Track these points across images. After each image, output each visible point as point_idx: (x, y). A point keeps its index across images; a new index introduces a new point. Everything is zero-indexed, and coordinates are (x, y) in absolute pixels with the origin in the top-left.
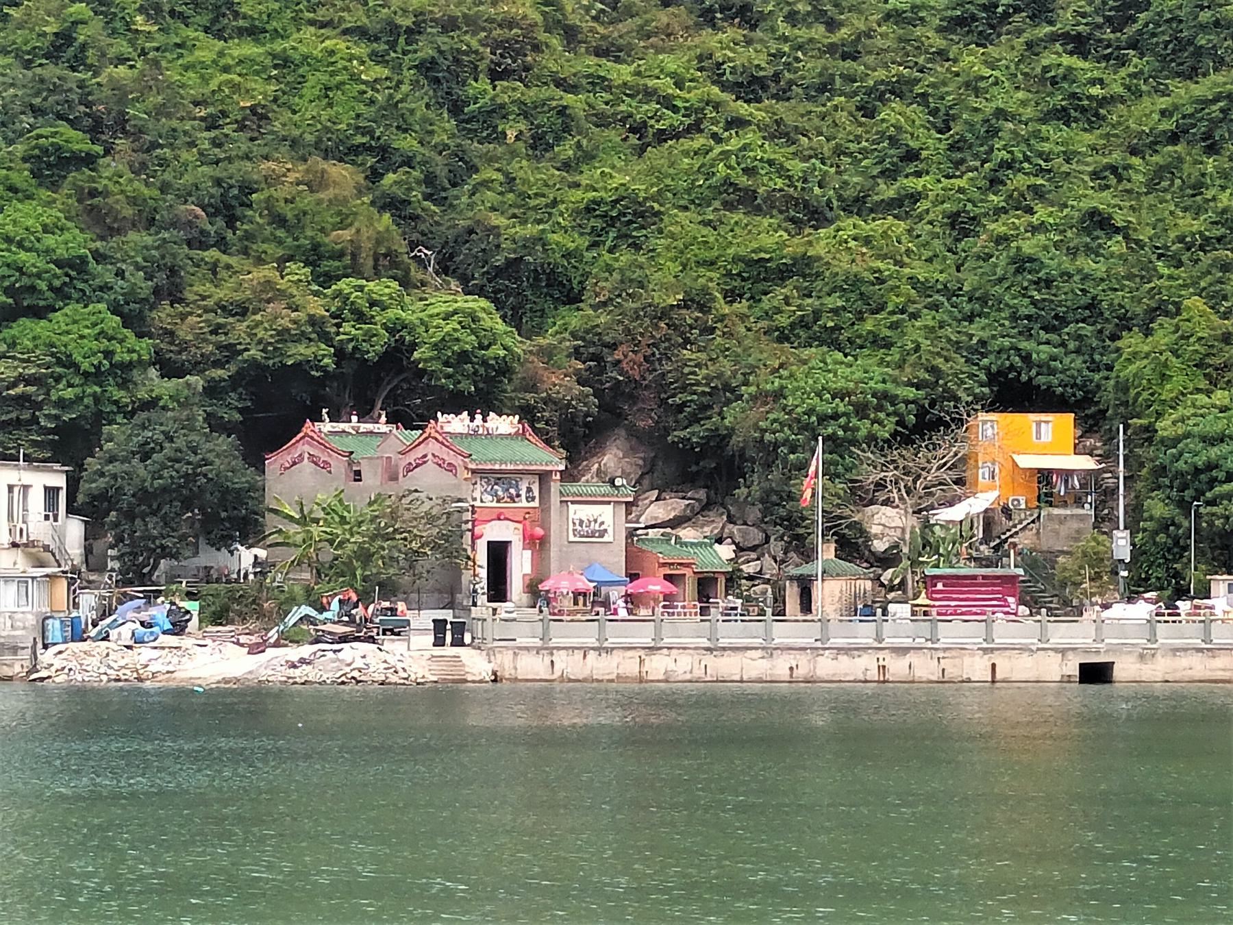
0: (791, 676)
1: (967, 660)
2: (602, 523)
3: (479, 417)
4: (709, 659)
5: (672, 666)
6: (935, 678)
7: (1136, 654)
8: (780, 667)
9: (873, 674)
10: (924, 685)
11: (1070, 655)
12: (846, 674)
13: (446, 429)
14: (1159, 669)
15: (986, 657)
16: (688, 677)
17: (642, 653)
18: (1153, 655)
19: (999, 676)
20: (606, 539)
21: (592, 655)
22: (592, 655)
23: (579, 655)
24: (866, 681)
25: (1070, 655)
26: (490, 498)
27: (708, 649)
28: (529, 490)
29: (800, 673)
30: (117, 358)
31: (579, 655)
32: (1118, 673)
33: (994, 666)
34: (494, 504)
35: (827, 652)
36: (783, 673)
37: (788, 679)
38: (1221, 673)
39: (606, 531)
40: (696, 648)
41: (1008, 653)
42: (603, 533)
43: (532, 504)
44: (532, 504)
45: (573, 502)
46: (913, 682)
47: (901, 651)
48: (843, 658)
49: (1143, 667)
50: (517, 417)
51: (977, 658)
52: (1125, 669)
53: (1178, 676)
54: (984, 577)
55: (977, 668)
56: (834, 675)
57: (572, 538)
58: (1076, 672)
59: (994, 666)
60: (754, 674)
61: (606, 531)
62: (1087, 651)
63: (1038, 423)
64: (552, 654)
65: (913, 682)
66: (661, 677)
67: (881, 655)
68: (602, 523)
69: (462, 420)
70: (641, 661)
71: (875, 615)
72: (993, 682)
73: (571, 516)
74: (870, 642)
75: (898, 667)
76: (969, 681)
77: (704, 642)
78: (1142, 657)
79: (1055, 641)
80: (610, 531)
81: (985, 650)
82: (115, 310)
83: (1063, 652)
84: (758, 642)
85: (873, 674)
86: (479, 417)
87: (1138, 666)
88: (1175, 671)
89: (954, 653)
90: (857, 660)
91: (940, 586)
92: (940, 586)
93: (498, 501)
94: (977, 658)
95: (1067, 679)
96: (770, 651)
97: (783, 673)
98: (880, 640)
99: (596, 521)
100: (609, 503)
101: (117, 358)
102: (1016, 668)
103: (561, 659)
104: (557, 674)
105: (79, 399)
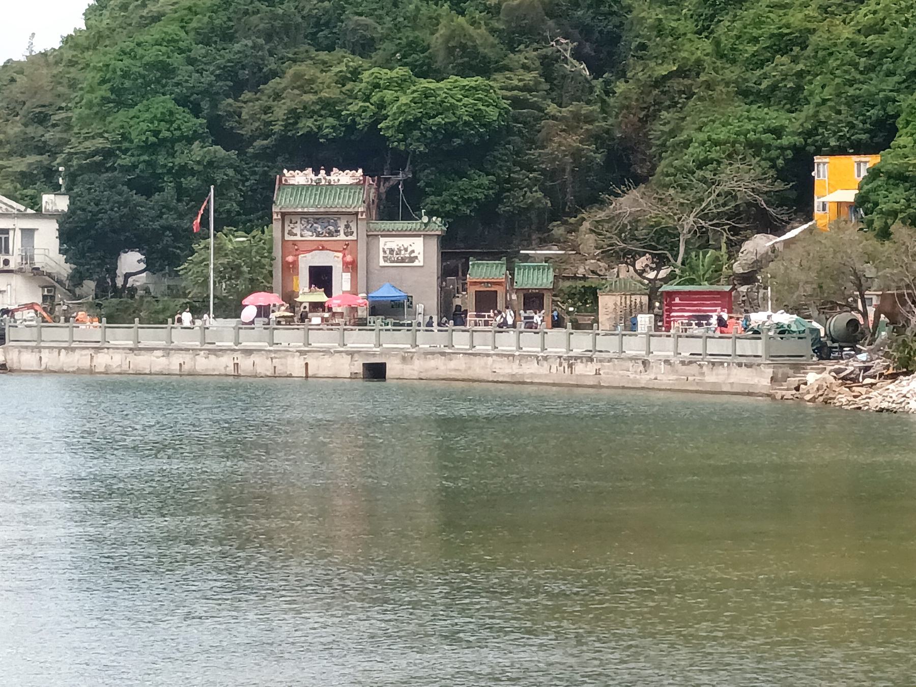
0: (180, 370)
1: (289, 360)
2: (413, 251)
3: (323, 172)
4: (132, 357)
5: (109, 362)
6: (269, 374)
7: (400, 356)
9: (231, 370)
11: (356, 357)
12: (214, 370)
13: (291, 182)
14: (416, 369)
15: (302, 357)
16: (118, 370)
17: (92, 352)
18: (412, 358)
19: (310, 373)
20: (416, 263)
23: (56, 352)
24: (227, 375)
25: (356, 357)
26: (310, 233)
27: (131, 349)
28: (347, 226)
29: (186, 368)
31: (56, 352)
32: (389, 373)
33: (307, 364)
34: (314, 238)
35: (202, 353)
37: (178, 372)
38: (453, 373)
39: (416, 257)
40: (124, 349)
41: (316, 354)
42: (412, 259)
43: (350, 238)
44: (350, 238)
45: (382, 236)
46: (256, 376)
47: (248, 352)
48: (212, 357)
49: (405, 367)
50: (360, 171)
51: (296, 359)
52: (394, 368)
55: (295, 366)
56: (207, 369)
57: (382, 263)
59: (307, 364)
60: (156, 369)
61: (416, 257)
62: (367, 354)
63: (859, 164)
64: (40, 352)
65: (256, 376)
66: (102, 370)
67: (236, 355)
68: (413, 251)
69: (306, 175)
70: (92, 357)
71: (167, 323)
72: (307, 377)
73: (381, 245)
74: (231, 344)
75: (246, 364)
76: (290, 376)
77: (130, 344)
78: (404, 359)
79: (350, 346)
80: (421, 257)
81: (302, 353)
83: (351, 354)
84: (162, 344)
85: (231, 370)
86: (323, 172)
87: (401, 366)
88: (426, 371)
89: (282, 355)
90: (221, 359)
91: (677, 300)
92: (677, 300)
93: (317, 236)
94: (296, 359)
95: (354, 376)
96: (167, 351)
97: (175, 368)
98: (237, 343)
99: (406, 250)
100: (419, 236)
102: (322, 366)
103: (45, 354)
104: (43, 367)
105: (134, 166)
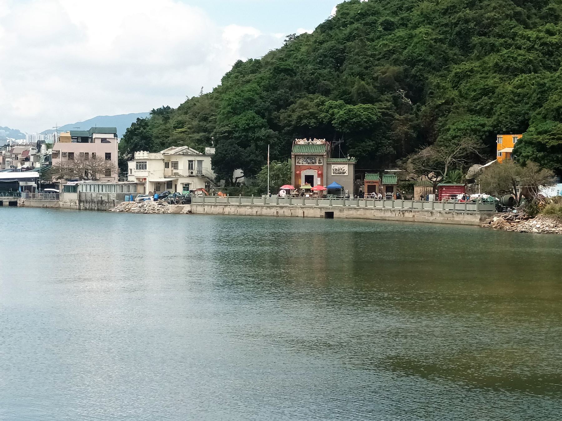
3: (310, 140)
4: (238, 209)
5: (230, 210)
8: (254, 211)
10: (351, 219)
11: (322, 209)
14: (345, 214)
21: (213, 207)
22: (213, 207)
25: (322, 209)
28: (319, 160)
29: (259, 213)
30: (250, 125)
36: (254, 213)
42: (344, 173)
47: (282, 207)
52: (336, 214)
53: (349, 217)
54: (456, 186)
55: (299, 213)
57: (332, 174)
58: (324, 214)
62: (326, 208)
63: (514, 138)
75: (281, 212)
76: (298, 216)
77: (238, 204)
80: (347, 172)
82: (258, 113)
83: (321, 208)
86: (310, 140)
92: (444, 189)
95: (321, 217)
96: (251, 207)
97: (254, 213)
101: (250, 125)
103: (206, 207)
105: (240, 137)
